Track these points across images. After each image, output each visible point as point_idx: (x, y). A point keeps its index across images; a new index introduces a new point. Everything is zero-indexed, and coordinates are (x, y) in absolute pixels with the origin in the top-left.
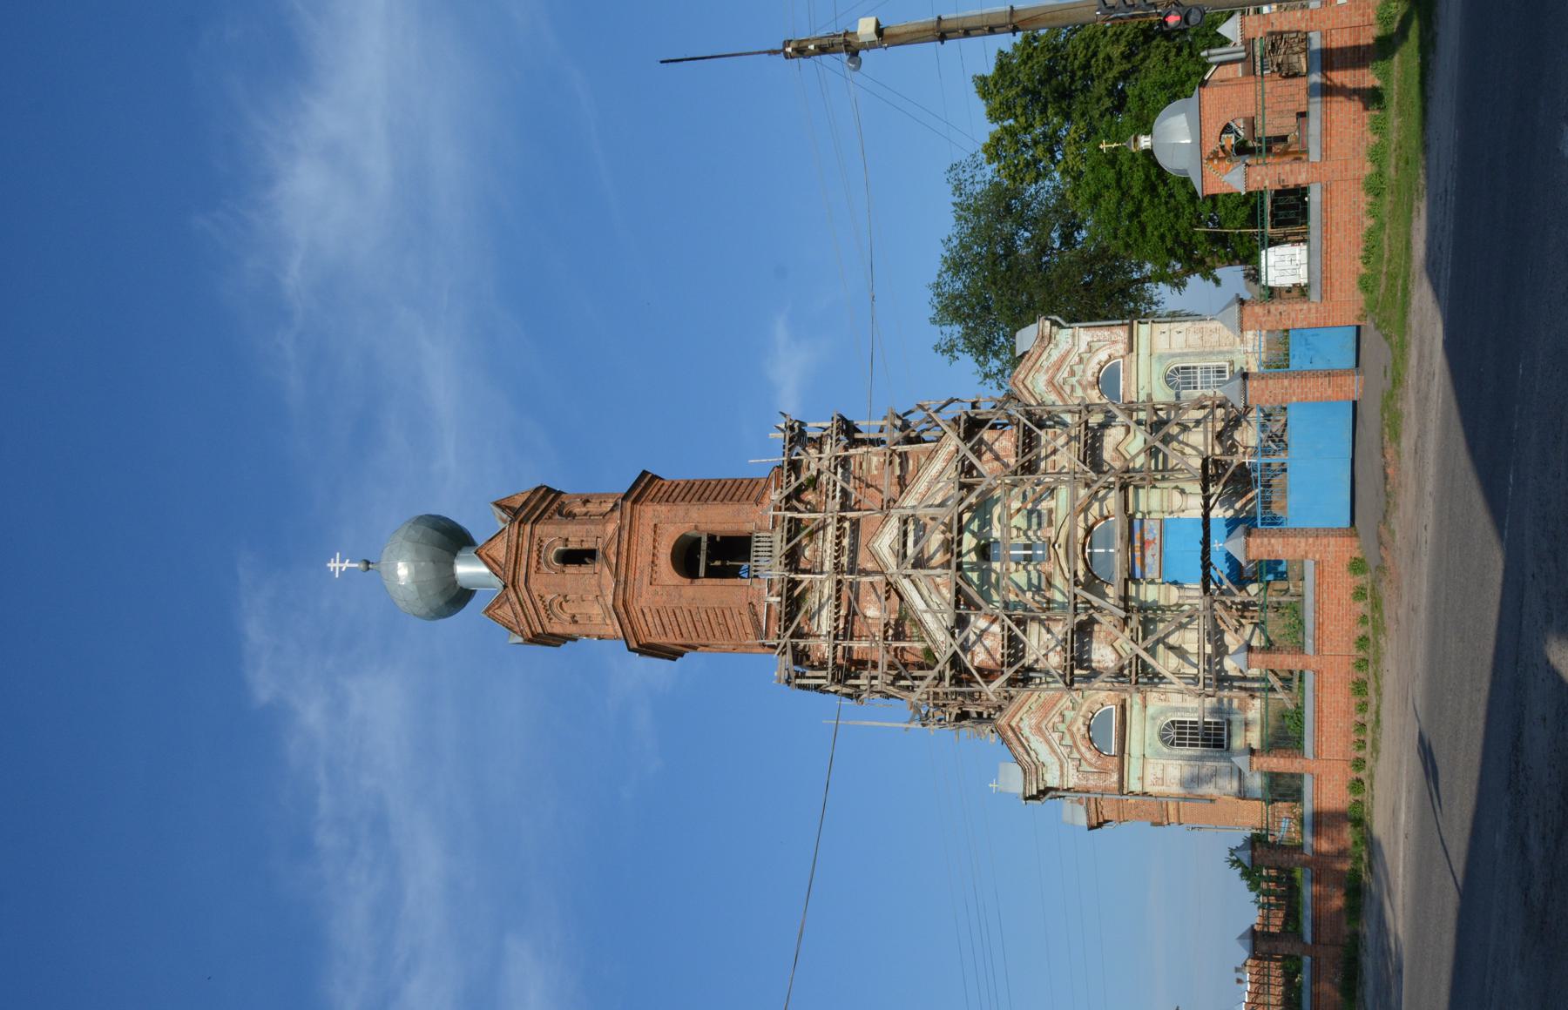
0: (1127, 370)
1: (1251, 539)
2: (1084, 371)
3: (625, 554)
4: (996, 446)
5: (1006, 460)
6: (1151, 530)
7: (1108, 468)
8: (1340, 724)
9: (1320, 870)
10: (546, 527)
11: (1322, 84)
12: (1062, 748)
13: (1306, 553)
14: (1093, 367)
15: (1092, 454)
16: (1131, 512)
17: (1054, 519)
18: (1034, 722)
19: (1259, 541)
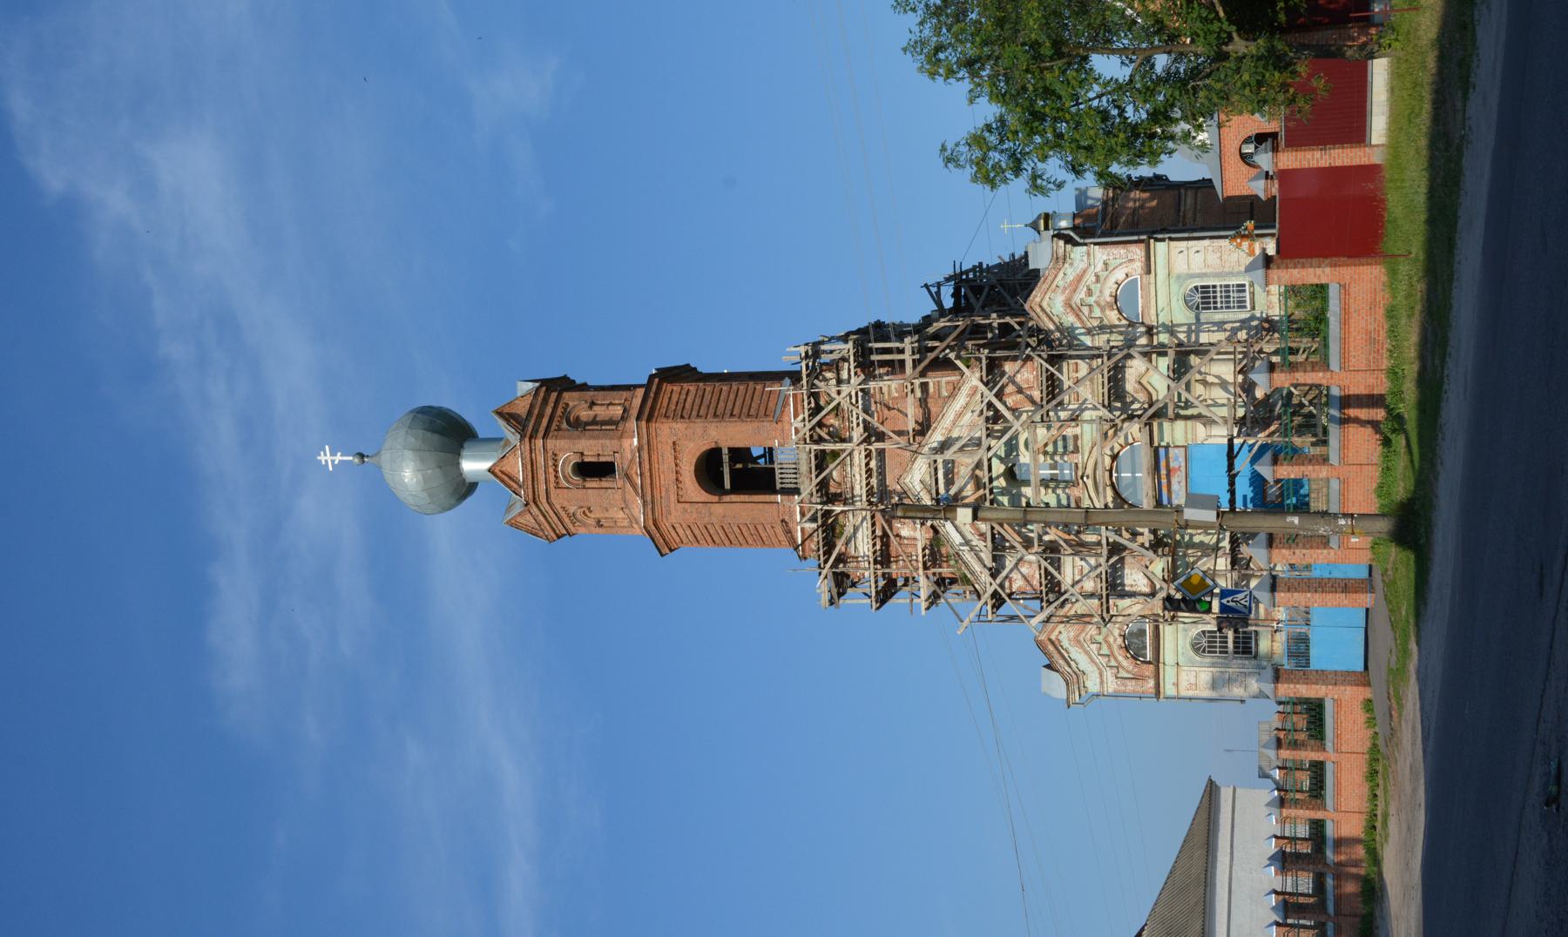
0: (1145, 288)
1: (1279, 685)
2: (1101, 292)
3: (648, 474)
4: (1018, 378)
5: (1029, 393)
6: (1176, 459)
7: (1131, 399)
8: (1357, 791)
11: (1340, 418)
12: (1099, 657)
14: (1109, 288)
15: (1116, 389)
16: (1156, 444)
17: (1080, 446)
18: (1072, 634)
19: (1286, 686)
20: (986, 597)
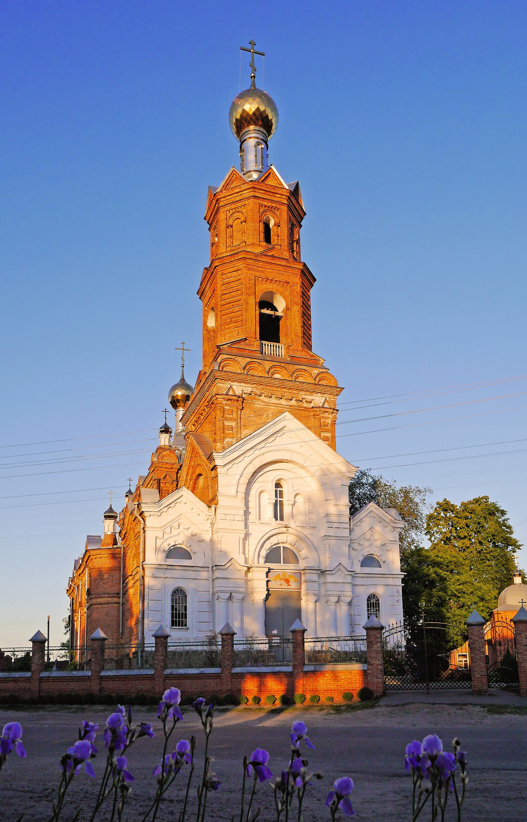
9: (154, 680)
10: (286, 213)
13: (372, 665)
20: (434, 509)
